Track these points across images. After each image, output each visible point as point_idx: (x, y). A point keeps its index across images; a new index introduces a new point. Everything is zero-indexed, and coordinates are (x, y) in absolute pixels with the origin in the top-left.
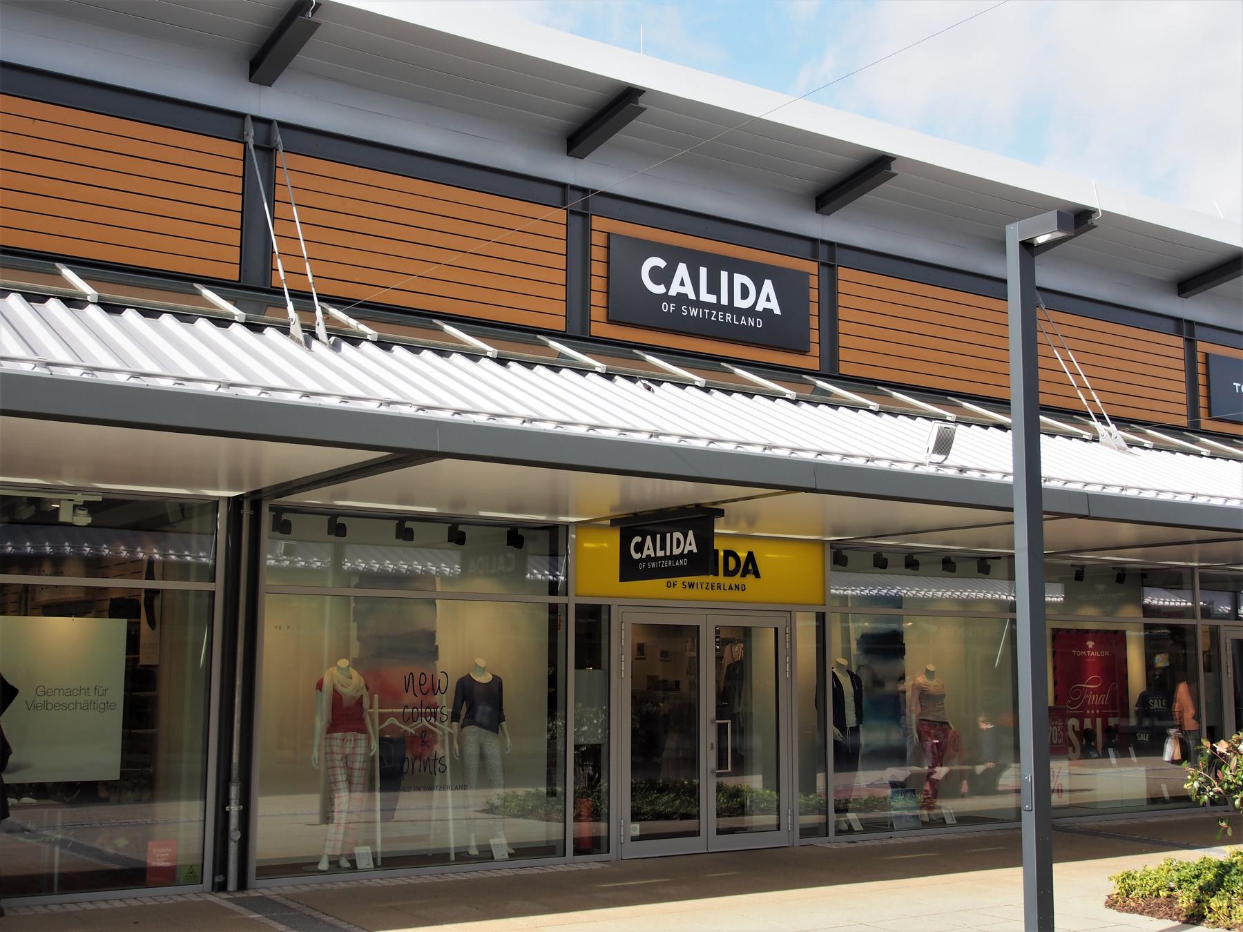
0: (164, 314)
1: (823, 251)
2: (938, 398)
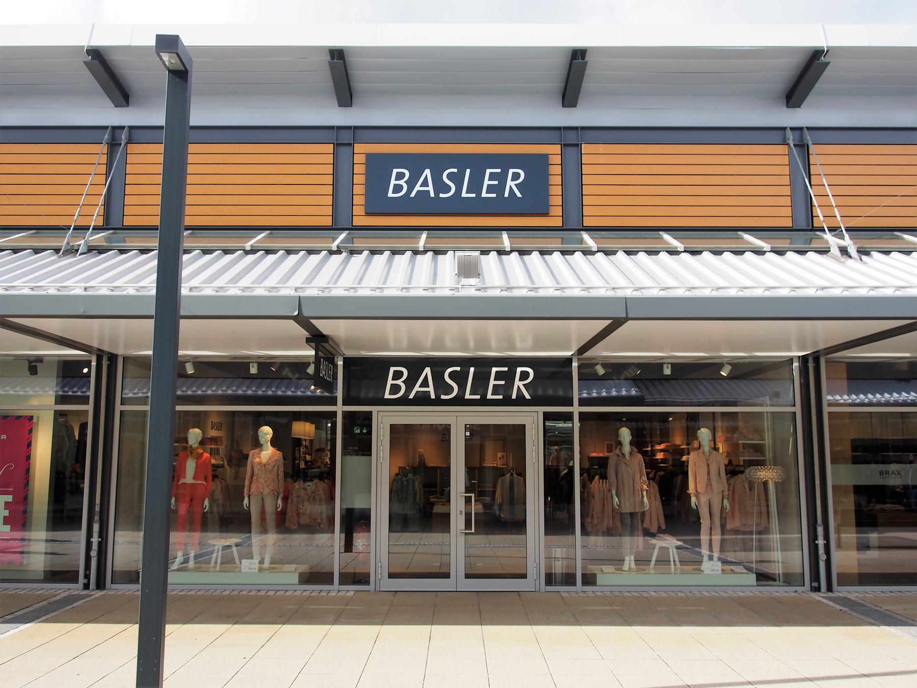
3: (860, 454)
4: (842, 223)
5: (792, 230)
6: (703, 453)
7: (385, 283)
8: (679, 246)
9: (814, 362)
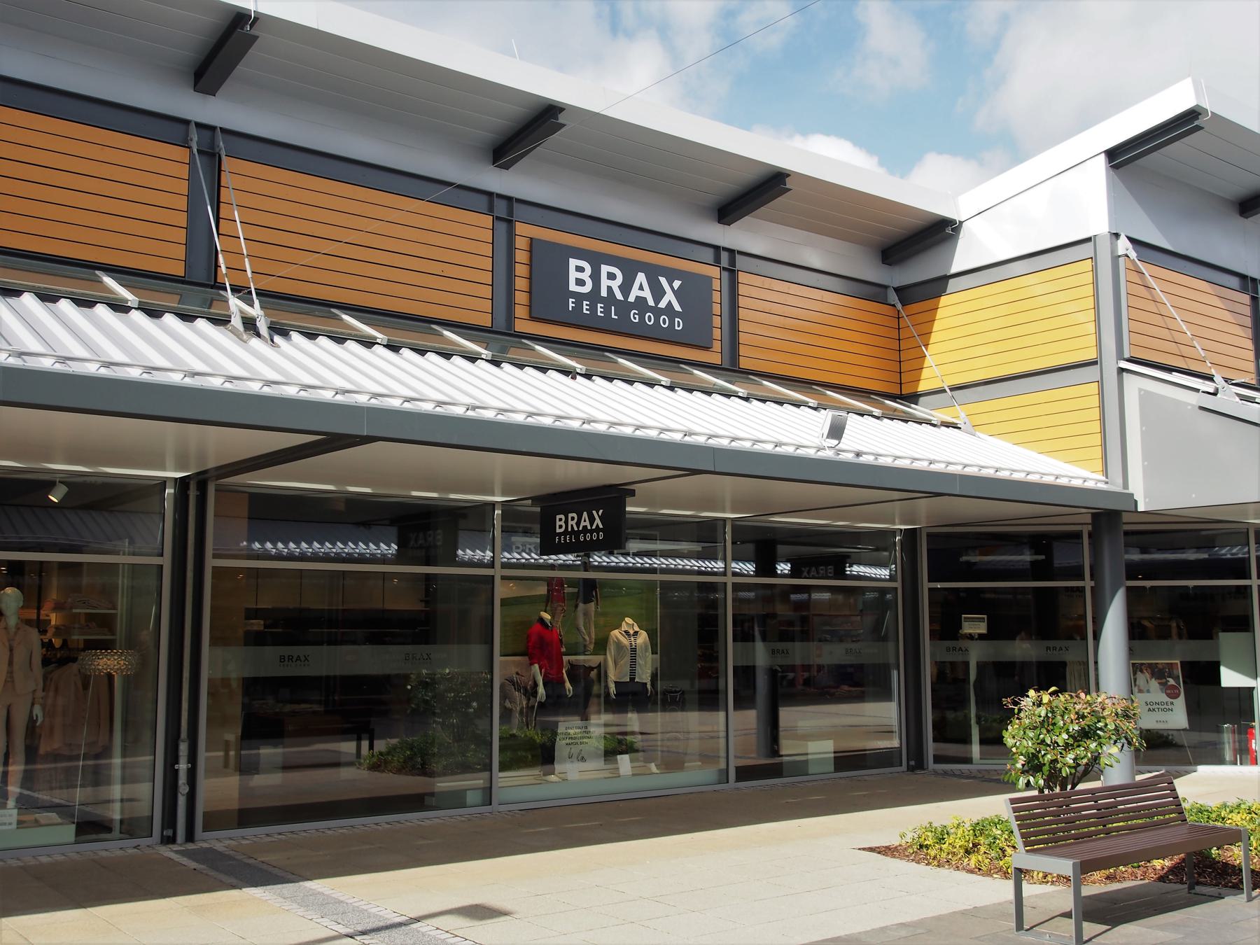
0: (199, 319)
1: (725, 257)
2: (279, 304)
3: (280, 630)
4: (253, 282)
5: (183, 282)
6: (6, 628)
9: (197, 490)
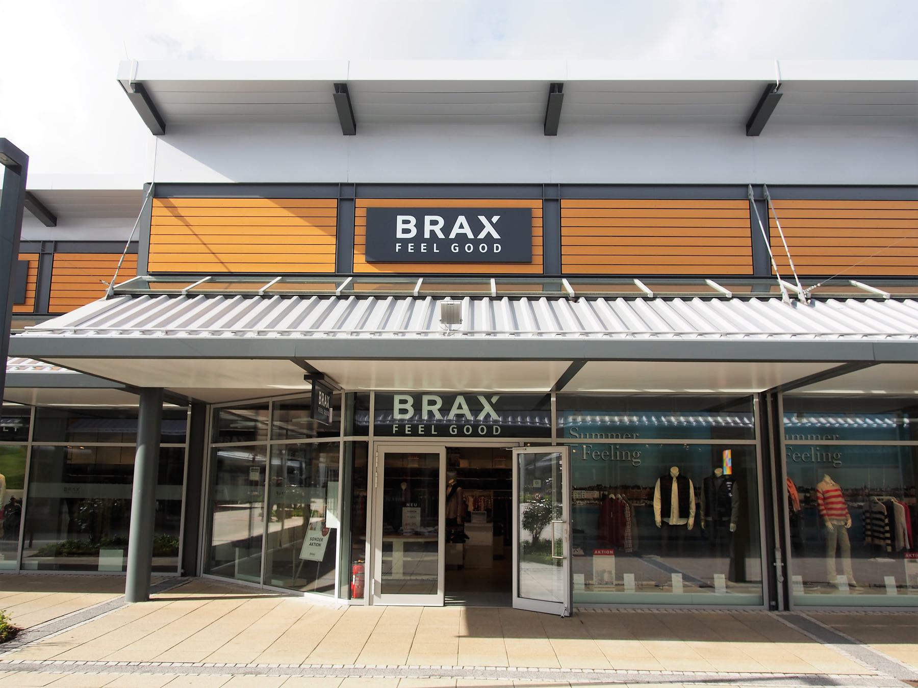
7: (406, 328)
8: (727, 293)
